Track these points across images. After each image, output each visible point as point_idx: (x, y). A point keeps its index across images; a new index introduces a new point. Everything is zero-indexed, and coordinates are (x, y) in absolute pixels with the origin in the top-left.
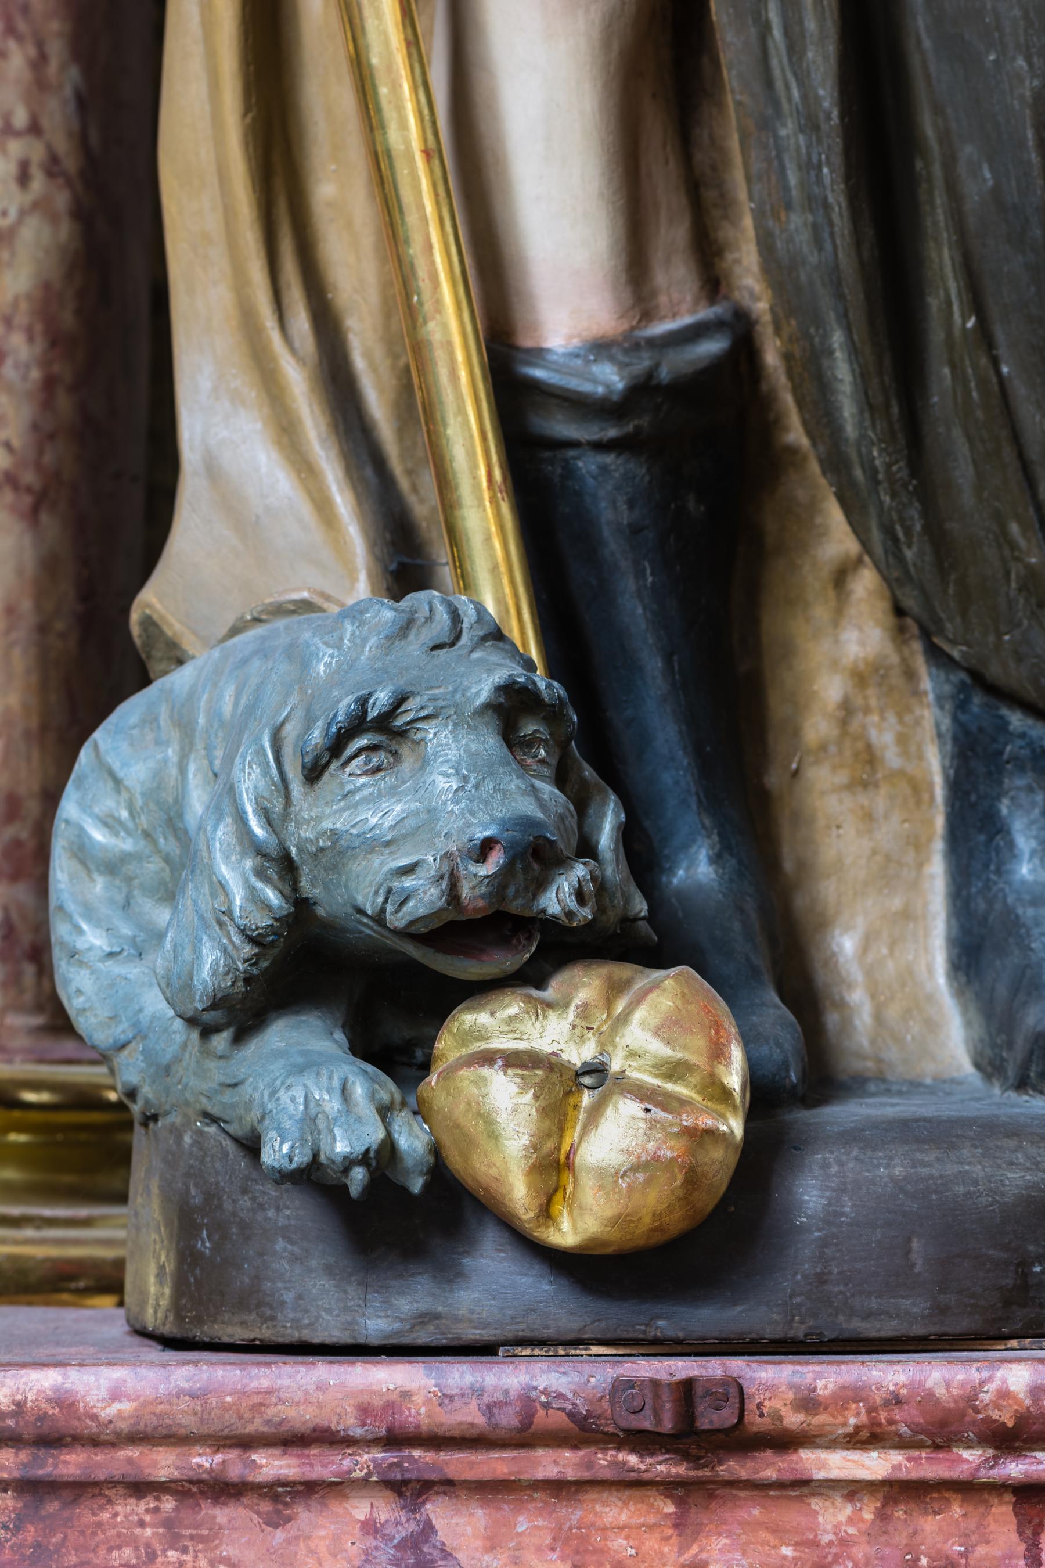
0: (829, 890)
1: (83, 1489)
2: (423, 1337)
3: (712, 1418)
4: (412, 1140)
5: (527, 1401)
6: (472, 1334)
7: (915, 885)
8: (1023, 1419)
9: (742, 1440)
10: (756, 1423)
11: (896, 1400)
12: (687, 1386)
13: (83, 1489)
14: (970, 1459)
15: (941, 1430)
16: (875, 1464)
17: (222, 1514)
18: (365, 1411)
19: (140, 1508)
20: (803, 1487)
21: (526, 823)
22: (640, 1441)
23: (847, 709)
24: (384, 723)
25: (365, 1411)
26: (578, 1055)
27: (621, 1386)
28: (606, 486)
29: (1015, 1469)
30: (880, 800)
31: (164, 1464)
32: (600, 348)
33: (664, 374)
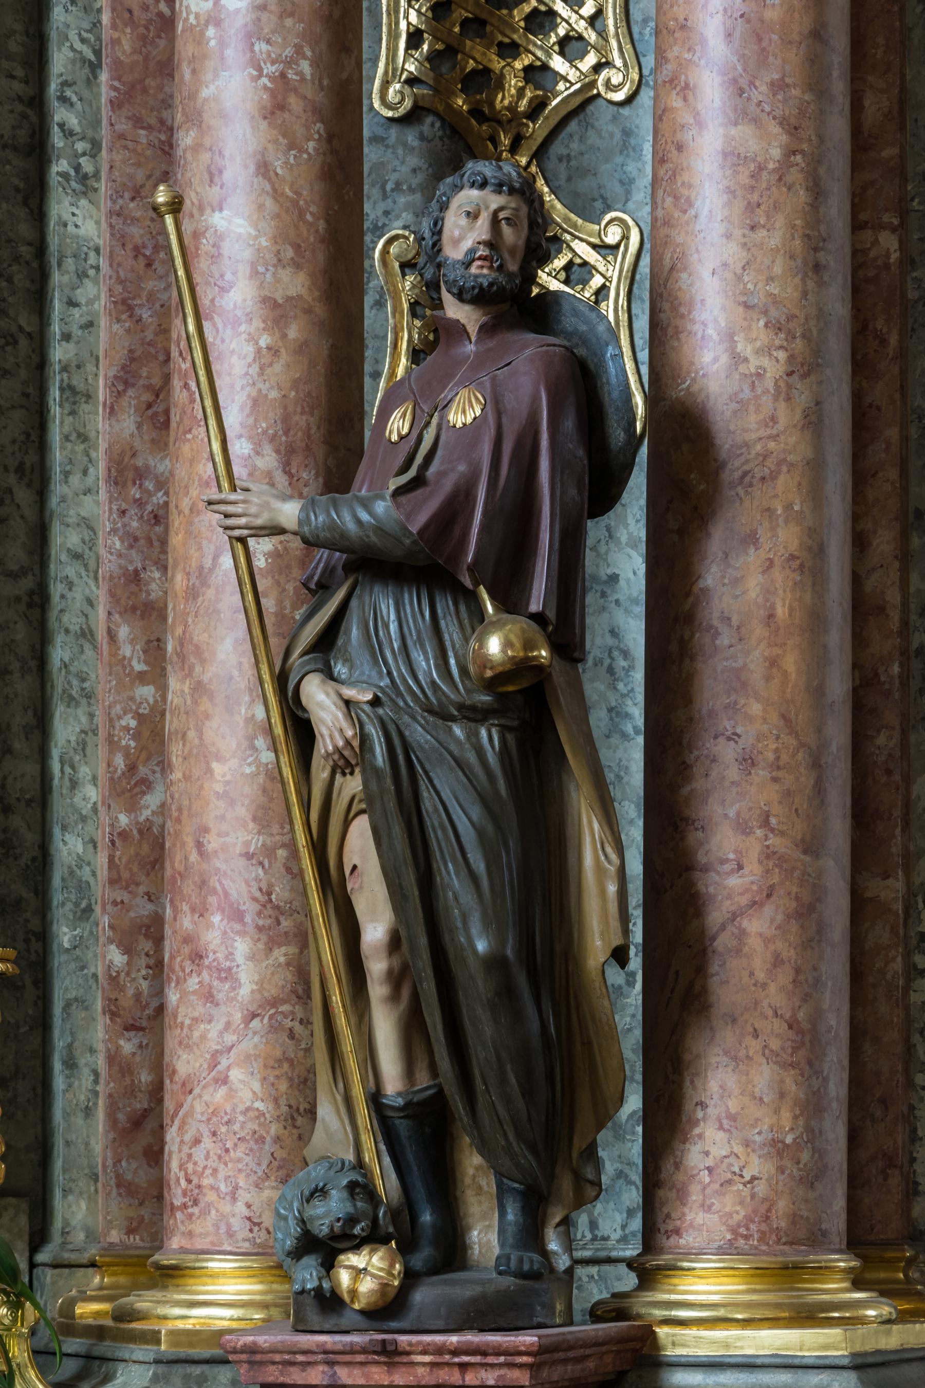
0: (470, 1220)
1: (262, 1363)
2: (335, 1329)
3: (390, 1348)
4: (326, 1285)
5: (351, 1343)
6: (344, 1329)
7: (491, 1219)
8: (456, 1349)
9: (397, 1352)
10: (400, 1349)
11: (429, 1344)
12: (384, 1341)
13: (262, 1363)
14: (447, 1357)
15: (439, 1350)
16: (427, 1359)
17: (292, 1369)
18: (318, 1346)
19: (274, 1367)
20: (413, 1364)
21: (348, 1213)
22: (375, 1353)
23: (474, 1176)
24: (322, 1190)
25: (318, 1346)
26: (362, 1266)
27: (371, 1340)
28: (402, 1126)
29: (456, 1360)
30: (483, 1199)
31: (278, 1358)
32: (399, 1094)
33: (415, 1100)
